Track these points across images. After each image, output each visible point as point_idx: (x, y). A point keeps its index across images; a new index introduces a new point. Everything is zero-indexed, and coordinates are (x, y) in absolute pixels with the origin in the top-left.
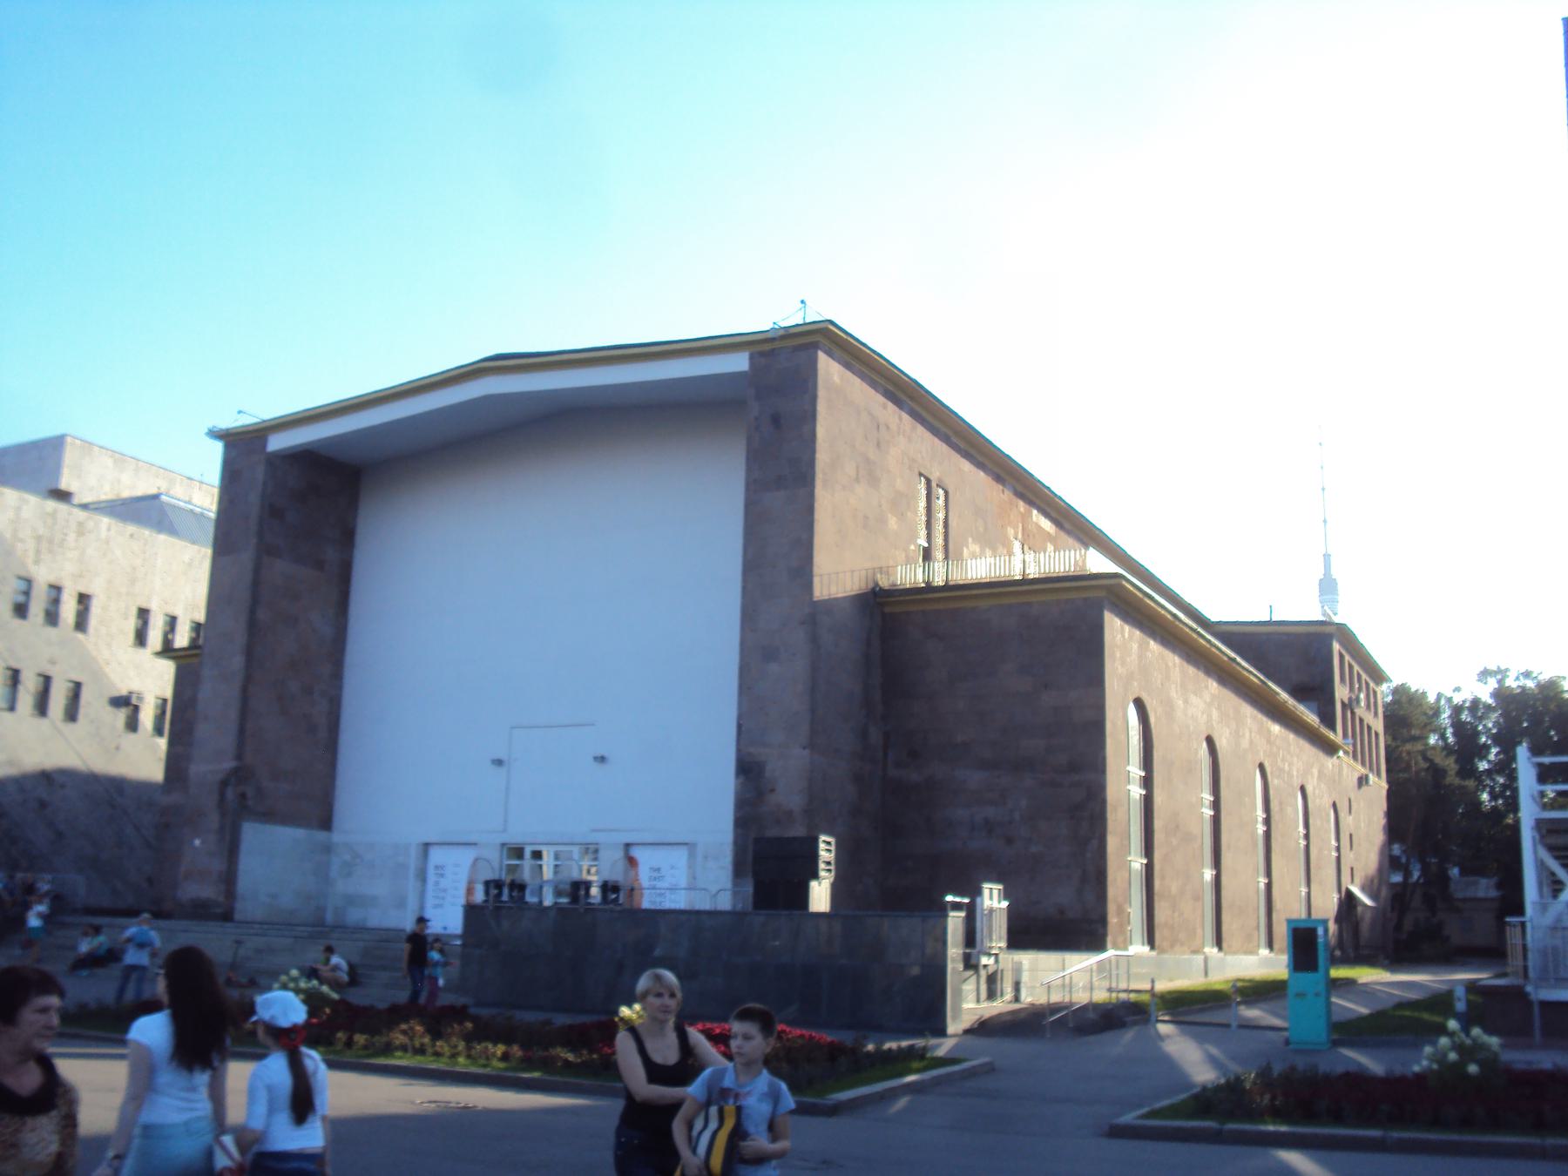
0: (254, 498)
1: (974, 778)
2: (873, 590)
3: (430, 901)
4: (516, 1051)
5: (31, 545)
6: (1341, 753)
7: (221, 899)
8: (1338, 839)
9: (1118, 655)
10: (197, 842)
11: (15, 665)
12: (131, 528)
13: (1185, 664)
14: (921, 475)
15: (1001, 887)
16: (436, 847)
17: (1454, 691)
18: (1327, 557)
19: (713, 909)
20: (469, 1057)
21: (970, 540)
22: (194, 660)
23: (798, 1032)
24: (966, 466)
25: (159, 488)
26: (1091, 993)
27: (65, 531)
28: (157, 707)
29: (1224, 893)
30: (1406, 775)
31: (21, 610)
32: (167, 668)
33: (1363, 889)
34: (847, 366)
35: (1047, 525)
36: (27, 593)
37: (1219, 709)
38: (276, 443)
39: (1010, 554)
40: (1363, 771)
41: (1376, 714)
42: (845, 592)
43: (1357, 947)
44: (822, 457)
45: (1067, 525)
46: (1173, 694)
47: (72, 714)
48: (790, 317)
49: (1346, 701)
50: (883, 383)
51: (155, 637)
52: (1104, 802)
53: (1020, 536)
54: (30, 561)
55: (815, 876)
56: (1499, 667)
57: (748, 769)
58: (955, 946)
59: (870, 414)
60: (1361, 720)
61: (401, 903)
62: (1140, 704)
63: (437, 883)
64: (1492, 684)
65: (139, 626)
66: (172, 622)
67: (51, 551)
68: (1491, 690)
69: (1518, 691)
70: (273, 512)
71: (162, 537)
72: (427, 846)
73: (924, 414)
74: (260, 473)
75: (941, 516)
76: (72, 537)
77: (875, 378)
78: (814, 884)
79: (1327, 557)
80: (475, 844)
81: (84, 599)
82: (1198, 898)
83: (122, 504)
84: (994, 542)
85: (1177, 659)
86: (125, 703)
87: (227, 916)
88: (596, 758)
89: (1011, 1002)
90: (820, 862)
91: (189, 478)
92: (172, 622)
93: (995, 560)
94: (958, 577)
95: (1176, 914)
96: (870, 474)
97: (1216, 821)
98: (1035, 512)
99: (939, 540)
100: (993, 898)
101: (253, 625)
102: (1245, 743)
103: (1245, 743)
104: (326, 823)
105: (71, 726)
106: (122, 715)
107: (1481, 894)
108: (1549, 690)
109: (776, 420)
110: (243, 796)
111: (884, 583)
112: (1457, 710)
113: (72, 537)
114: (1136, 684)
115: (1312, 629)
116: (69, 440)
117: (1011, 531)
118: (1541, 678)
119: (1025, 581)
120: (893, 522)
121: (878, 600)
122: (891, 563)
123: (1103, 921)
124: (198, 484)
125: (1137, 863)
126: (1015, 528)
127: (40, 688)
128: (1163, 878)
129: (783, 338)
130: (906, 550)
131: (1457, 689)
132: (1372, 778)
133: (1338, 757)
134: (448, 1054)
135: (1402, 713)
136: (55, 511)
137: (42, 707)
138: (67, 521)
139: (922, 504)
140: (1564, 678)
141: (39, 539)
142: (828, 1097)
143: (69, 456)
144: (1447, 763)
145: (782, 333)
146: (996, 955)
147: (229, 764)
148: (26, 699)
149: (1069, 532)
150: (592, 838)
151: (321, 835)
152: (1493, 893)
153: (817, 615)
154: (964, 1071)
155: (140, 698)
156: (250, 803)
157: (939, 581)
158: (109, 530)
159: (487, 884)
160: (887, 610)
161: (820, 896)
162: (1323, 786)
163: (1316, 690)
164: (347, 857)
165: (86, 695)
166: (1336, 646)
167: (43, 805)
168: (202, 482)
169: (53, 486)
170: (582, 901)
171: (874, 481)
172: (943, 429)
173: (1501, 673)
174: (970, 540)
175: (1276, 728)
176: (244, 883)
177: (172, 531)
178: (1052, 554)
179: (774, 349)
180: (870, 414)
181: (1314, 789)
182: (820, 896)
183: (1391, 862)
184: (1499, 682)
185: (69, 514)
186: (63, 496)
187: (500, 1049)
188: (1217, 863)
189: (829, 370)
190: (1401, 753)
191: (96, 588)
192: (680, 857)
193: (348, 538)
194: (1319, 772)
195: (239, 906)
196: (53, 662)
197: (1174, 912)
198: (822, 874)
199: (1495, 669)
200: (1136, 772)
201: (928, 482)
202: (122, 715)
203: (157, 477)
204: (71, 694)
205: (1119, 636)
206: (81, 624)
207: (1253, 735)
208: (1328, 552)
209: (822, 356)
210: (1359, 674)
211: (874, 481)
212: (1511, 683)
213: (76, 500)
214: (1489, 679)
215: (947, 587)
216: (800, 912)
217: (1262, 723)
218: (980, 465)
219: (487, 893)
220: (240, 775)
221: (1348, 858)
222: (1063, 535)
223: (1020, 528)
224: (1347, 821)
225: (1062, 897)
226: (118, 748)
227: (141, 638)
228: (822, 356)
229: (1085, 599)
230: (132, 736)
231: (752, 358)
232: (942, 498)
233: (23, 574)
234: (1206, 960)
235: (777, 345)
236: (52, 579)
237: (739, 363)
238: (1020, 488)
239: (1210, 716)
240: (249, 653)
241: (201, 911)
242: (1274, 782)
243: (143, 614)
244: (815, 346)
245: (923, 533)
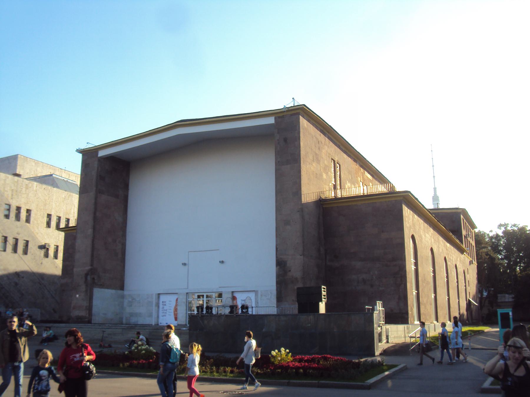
0: (94, 173)
1: (358, 264)
2: (320, 199)
3: (161, 314)
4: (236, 370)
5: (10, 193)
6: (465, 253)
7: (87, 315)
8: (465, 283)
9: (407, 220)
10: (77, 296)
11: (5, 235)
12: (44, 186)
13: (424, 223)
14: (332, 159)
15: (381, 302)
16: (236, 293)
17: (490, 232)
18: (435, 189)
19: (257, 314)
20: (217, 372)
21: (347, 182)
22: (75, 231)
23: (336, 358)
24: (345, 156)
25: (51, 172)
26: (103, 335)
27: (22, 187)
28: (54, 249)
29: (438, 302)
30: (481, 260)
32: (61, 235)
33: (473, 299)
34: (309, 121)
35: (369, 176)
36: (9, 210)
37: (433, 238)
38: (102, 153)
39: (359, 186)
40: (471, 259)
41: (473, 240)
42: (307, 201)
43: (472, 319)
44: (302, 153)
45: (375, 177)
46: (422, 233)
47: (25, 252)
48: (289, 104)
49: (465, 235)
50: (320, 127)
51: (53, 223)
52: (405, 271)
53: (362, 181)
54: (9, 198)
55: (321, 301)
56: (505, 223)
57: (281, 264)
58: (376, 324)
59: (316, 138)
60: (469, 242)
61: (151, 315)
62: (413, 237)
63: (163, 308)
64: (503, 229)
65: (48, 220)
66: (59, 218)
68: (502, 231)
69: (512, 231)
70: (101, 178)
71: (55, 189)
72: (159, 294)
73: (332, 138)
74: (96, 164)
75: (338, 173)
76: (24, 189)
77: (317, 125)
78: (320, 303)
79: (435, 189)
80: (177, 293)
81: (28, 211)
82: (431, 304)
83: (39, 178)
84: (354, 182)
85: (422, 221)
86: (44, 247)
87: (89, 322)
88: (220, 262)
89: (386, 343)
90: (322, 295)
91: (61, 169)
92: (59, 218)
93: (355, 189)
94: (345, 194)
95: (426, 310)
96: (317, 159)
97: (434, 277)
98: (366, 172)
99: (338, 182)
100: (379, 307)
101: (95, 219)
102: (441, 250)
103: (441, 250)
104: (122, 288)
105: (25, 256)
106: (43, 252)
107: (507, 300)
108: (522, 230)
109: (285, 140)
110: (94, 279)
111: (323, 197)
112: (491, 238)
113: (24, 189)
114: (412, 230)
115: (454, 211)
116: (19, 156)
117: (359, 179)
118: (519, 226)
119: (364, 196)
120: (324, 176)
121: (321, 203)
122: (325, 190)
123: (407, 313)
124: (64, 171)
125: (415, 292)
126: (360, 177)
127: (14, 243)
128: (422, 298)
129: (287, 111)
130: (329, 185)
131: (491, 231)
132: (474, 262)
133: (464, 254)
134: (209, 372)
135: (479, 239)
136: (18, 181)
137: (15, 250)
138: (22, 184)
139: (333, 169)
140: (527, 226)
141: (12, 190)
142: (366, 382)
143: (19, 162)
144: (495, 256)
145: (287, 109)
146: (381, 326)
147: (88, 268)
148: (9, 247)
149: (376, 179)
150: (220, 290)
151: (120, 292)
152: (511, 300)
153: (303, 208)
154: (400, 369)
155: (49, 246)
156: (96, 281)
157: (339, 196)
158: (36, 187)
159: (198, 308)
160: (324, 206)
161: (322, 308)
162: (461, 264)
163: (457, 232)
164: (130, 300)
165: (30, 245)
166: (462, 217)
167: (16, 284)
168: (65, 170)
169: (14, 173)
170: (235, 313)
171: (318, 161)
172: (338, 143)
173: (506, 225)
174: (347, 182)
175: (448, 245)
176: (95, 310)
177: (57, 186)
178: (371, 186)
179: (283, 115)
180: (316, 138)
181: (459, 265)
182: (322, 308)
183: (480, 291)
184: (505, 228)
185: (23, 181)
186: (19, 175)
187: (229, 369)
188: (435, 292)
189: (303, 122)
190: (479, 252)
191: (32, 207)
192: (252, 296)
193: (126, 187)
194: (460, 259)
195: (93, 318)
196: (18, 234)
197: (425, 309)
198: (323, 299)
199: (504, 224)
200: (413, 261)
201: (334, 161)
202: (43, 252)
203: (50, 168)
204: (25, 245)
205: (407, 213)
206: (28, 220)
207: (443, 247)
208: (436, 187)
209: (301, 118)
210: (468, 226)
211: (318, 161)
212: (509, 228)
213: (22, 177)
214: (501, 227)
215: (341, 198)
216: (316, 314)
217: (445, 243)
218: (349, 156)
219: (198, 311)
220: (92, 271)
221: (468, 289)
222: (374, 180)
223: (362, 177)
224: (467, 276)
226: (42, 263)
227: (48, 225)
228: (301, 118)
229: (396, 200)
230: (46, 259)
231: (275, 119)
232: (338, 167)
233: (8, 203)
234: (435, 325)
235: (285, 113)
236: (18, 205)
237: (271, 120)
238: (361, 164)
239: (431, 241)
240: (94, 228)
241: (80, 320)
242: (449, 263)
243: (49, 216)
244: (298, 114)
245: (333, 179)
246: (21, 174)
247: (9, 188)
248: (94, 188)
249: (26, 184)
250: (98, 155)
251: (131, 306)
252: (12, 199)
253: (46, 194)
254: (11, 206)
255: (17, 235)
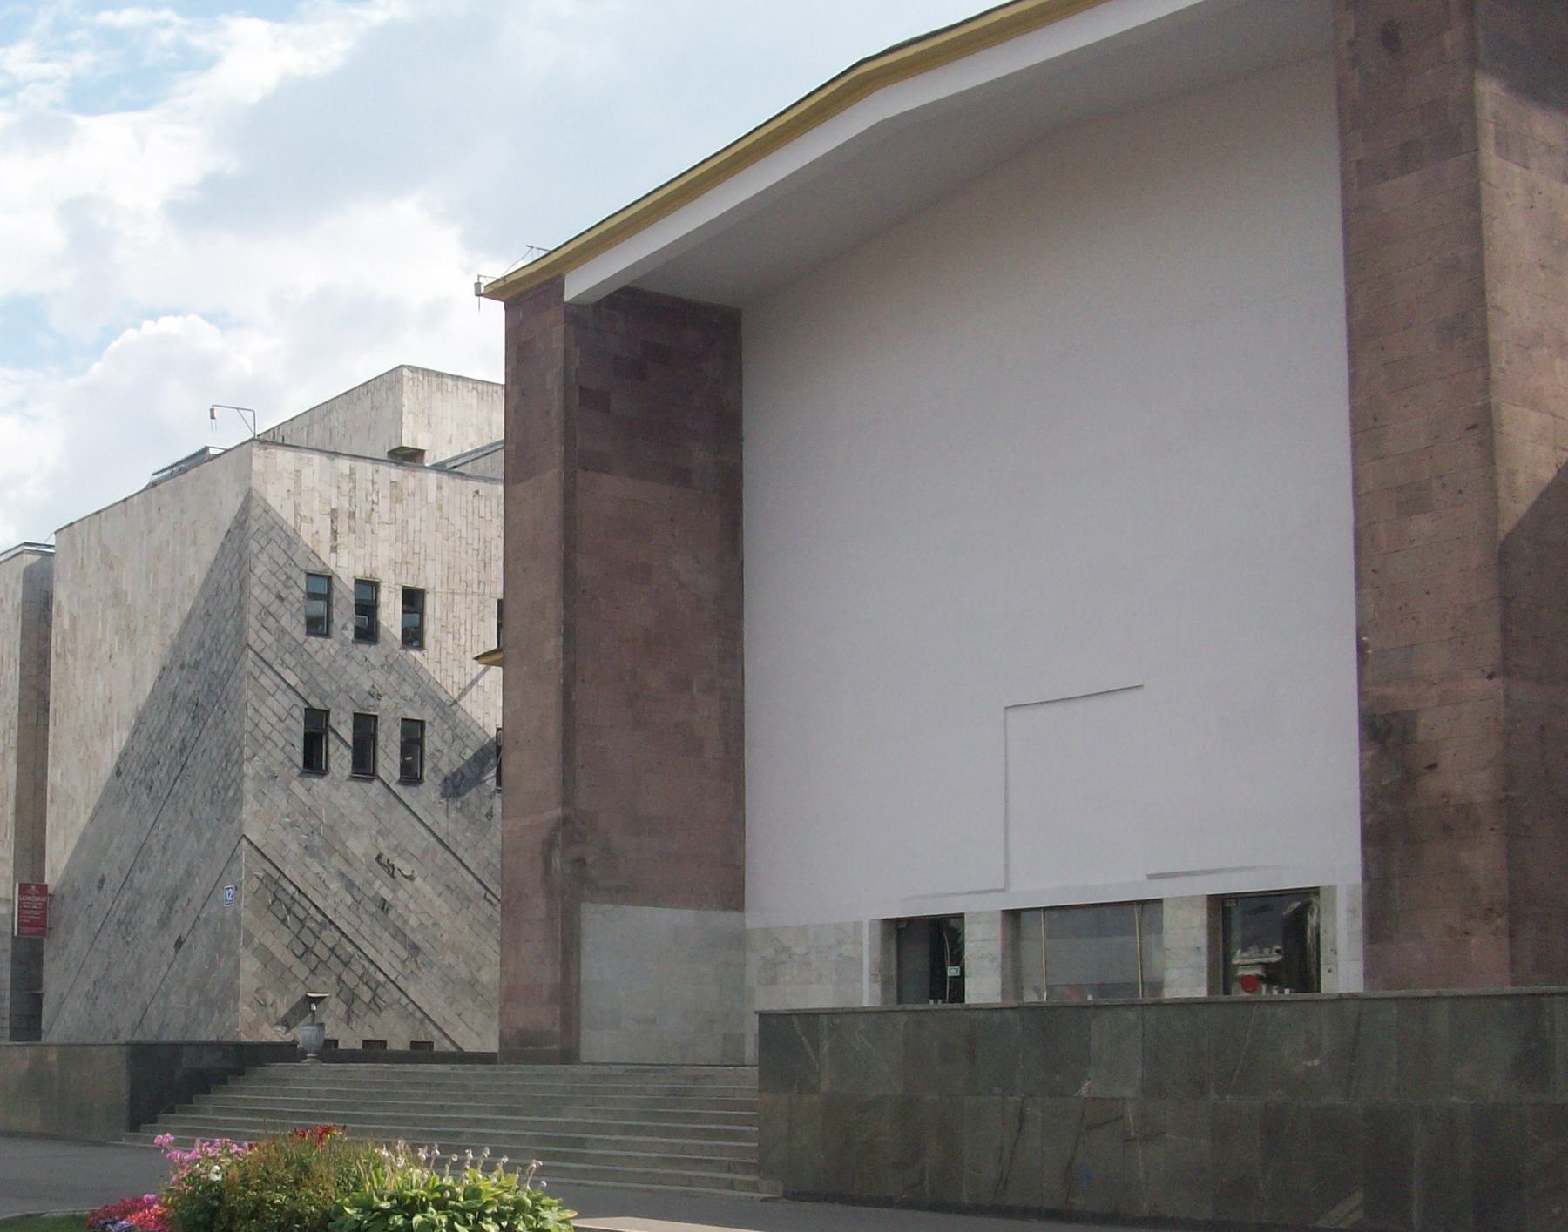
0: (553, 380)
5: (324, 526)
7: (557, 1028)
31: (318, 626)
54: (324, 552)
67: (352, 530)
76: (384, 505)
81: (413, 599)
104: (733, 896)
110: (581, 861)
113: (384, 505)
147: (554, 813)
148: (340, 758)
151: (722, 920)
164: (770, 953)
191: (428, 578)
206: (413, 636)
225: (292, 1023)
233: (315, 568)
240: (568, 632)
246: (420, 447)
247: (316, 504)
248: (559, 449)
249: (392, 482)
250: (562, 294)
251: (773, 981)
252: (334, 549)
253: (489, 517)
254: (335, 580)
255: (372, 702)
